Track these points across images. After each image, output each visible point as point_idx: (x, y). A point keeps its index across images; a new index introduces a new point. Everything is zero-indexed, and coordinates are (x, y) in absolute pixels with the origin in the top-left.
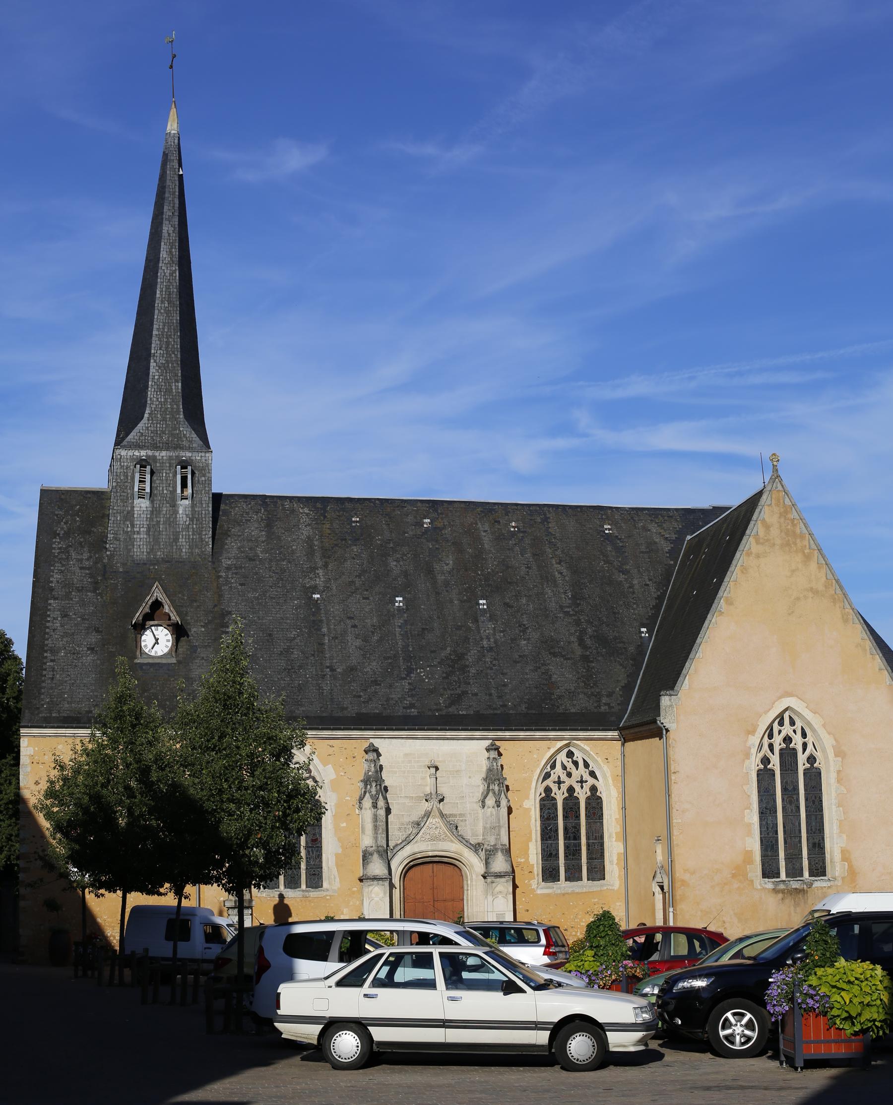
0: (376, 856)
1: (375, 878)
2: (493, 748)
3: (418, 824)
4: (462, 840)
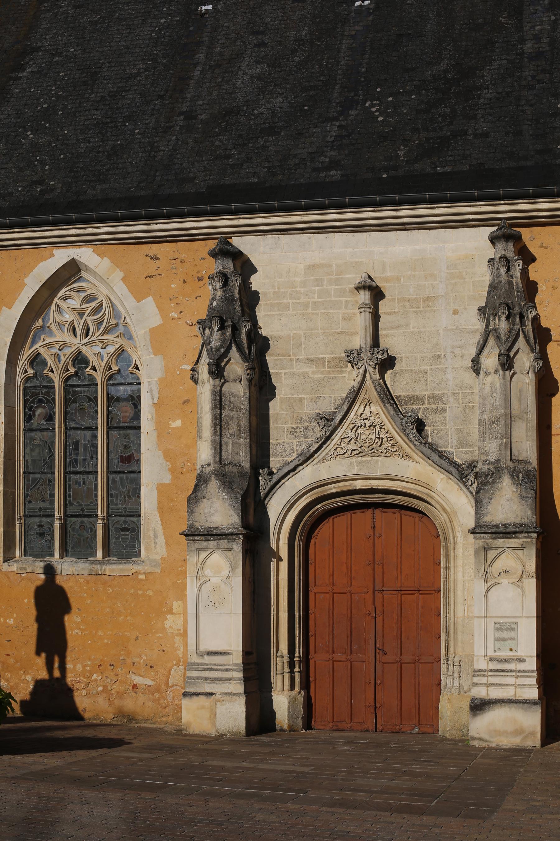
0: (214, 485)
1: (212, 534)
2: (507, 234)
3: (329, 423)
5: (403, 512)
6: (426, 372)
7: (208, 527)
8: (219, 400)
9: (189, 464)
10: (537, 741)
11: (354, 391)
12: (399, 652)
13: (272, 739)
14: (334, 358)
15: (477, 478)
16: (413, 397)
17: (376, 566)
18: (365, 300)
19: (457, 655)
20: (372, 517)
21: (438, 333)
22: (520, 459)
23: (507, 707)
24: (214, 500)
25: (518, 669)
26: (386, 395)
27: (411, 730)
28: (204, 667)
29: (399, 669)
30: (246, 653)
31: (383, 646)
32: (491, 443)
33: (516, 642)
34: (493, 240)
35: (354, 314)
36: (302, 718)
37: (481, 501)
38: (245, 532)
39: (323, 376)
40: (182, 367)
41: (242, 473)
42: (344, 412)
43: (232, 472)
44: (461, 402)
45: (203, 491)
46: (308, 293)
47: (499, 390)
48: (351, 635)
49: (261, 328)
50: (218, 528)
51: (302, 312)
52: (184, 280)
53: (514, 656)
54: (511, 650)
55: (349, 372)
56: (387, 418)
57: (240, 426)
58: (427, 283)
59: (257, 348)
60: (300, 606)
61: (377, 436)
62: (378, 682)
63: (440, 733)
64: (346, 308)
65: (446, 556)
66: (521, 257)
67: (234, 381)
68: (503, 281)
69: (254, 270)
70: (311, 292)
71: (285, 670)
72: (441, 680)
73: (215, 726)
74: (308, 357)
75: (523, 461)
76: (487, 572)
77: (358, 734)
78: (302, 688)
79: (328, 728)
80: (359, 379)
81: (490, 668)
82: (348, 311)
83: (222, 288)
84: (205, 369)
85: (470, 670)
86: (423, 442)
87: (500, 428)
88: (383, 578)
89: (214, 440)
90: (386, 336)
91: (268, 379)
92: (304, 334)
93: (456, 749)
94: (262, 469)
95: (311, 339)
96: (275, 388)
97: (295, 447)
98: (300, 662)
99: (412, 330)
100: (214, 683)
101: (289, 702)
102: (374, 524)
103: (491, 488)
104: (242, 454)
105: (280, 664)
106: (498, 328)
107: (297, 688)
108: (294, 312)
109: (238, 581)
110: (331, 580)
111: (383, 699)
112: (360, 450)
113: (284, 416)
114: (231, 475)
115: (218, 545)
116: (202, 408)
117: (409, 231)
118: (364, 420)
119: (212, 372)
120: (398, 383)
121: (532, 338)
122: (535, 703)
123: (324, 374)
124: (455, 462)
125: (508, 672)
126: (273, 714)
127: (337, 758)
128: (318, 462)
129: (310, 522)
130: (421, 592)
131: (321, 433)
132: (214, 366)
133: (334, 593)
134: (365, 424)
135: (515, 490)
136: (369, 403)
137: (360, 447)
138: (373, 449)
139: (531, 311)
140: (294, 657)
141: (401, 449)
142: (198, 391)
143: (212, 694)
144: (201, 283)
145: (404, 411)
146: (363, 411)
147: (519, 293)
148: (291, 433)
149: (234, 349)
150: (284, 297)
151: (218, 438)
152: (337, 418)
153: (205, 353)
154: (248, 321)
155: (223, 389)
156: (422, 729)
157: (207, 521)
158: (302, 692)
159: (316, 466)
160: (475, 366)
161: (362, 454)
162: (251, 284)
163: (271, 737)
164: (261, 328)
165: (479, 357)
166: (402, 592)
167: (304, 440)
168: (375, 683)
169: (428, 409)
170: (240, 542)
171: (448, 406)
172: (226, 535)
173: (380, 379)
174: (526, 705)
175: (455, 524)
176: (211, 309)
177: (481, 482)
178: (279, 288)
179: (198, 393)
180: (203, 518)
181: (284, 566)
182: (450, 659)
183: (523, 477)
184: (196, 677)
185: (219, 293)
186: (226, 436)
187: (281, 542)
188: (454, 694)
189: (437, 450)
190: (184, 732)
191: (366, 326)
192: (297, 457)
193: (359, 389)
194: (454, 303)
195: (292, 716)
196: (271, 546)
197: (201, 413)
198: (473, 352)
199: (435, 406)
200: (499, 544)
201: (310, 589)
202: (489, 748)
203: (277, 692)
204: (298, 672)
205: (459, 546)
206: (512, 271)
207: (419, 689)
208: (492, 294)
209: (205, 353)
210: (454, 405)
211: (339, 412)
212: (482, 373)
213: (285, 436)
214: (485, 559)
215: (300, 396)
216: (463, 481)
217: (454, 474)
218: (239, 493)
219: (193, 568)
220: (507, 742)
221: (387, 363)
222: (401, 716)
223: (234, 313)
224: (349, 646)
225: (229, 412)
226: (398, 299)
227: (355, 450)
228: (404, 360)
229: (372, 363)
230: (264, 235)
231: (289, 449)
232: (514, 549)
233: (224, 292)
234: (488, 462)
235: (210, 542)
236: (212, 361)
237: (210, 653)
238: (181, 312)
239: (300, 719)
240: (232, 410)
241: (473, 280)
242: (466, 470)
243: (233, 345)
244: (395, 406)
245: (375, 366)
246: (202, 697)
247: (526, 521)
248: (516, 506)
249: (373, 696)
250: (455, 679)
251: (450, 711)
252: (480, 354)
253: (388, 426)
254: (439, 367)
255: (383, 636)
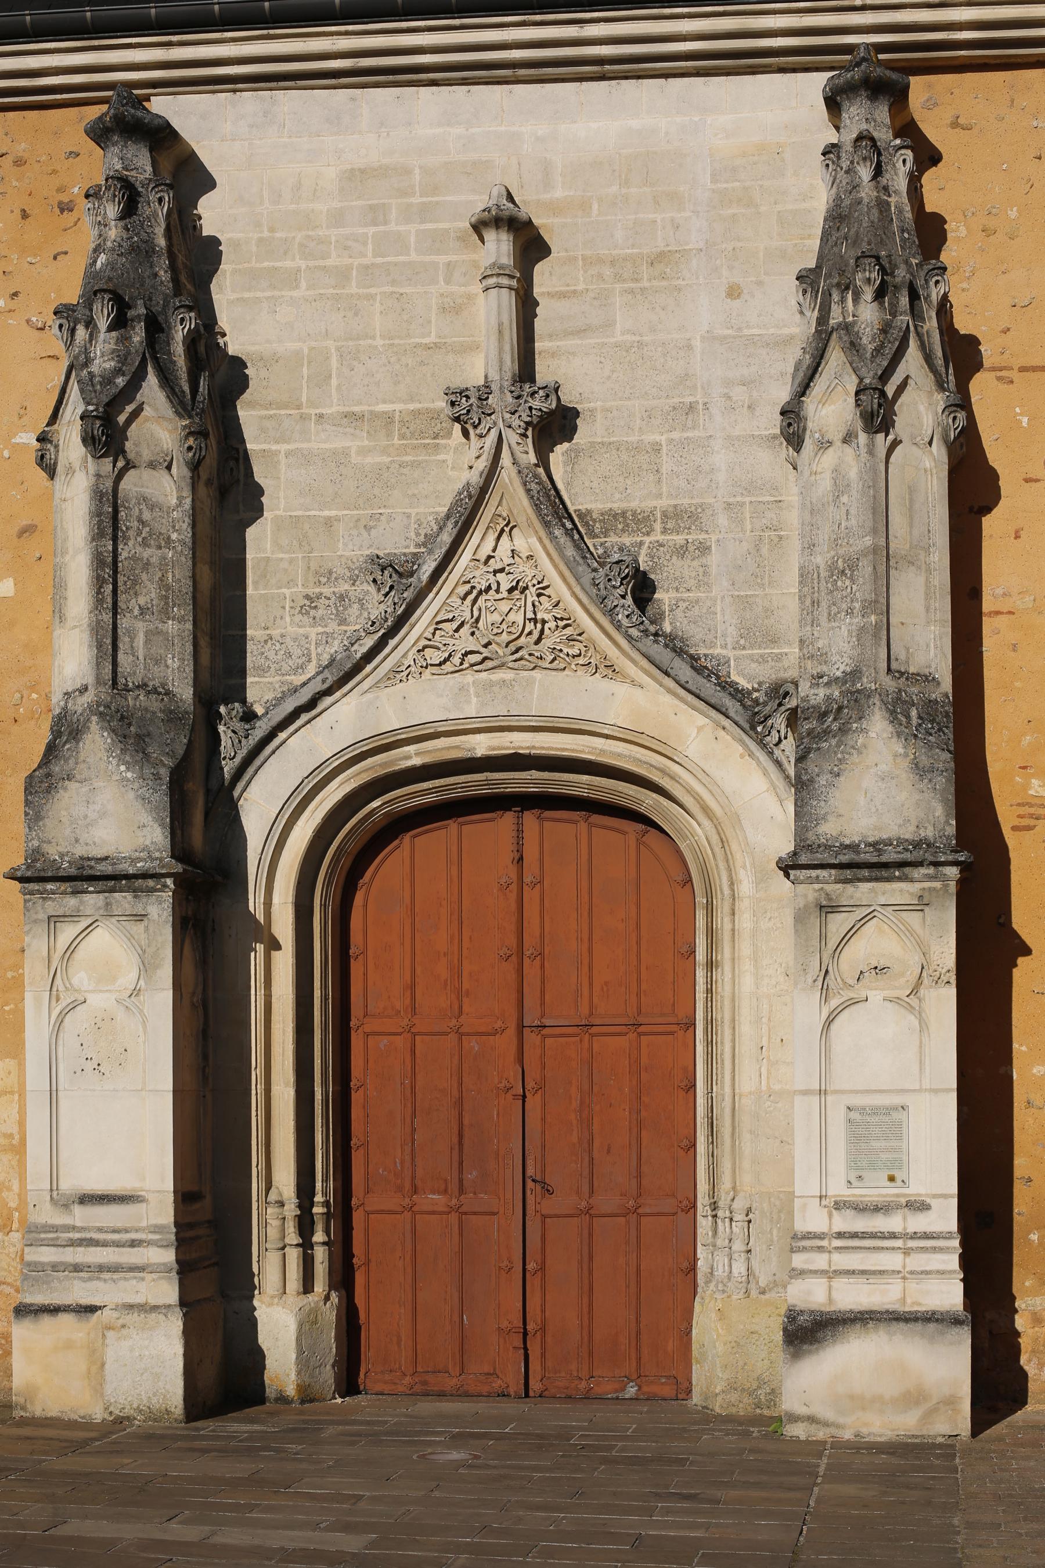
0: (96, 744)
3: (405, 584)
4: (703, 680)
5: (596, 818)
6: (656, 448)
7: (82, 858)
8: (110, 517)
9: (34, 696)
10: (963, 1424)
11: (470, 497)
12: (586, 1188)
13: (256, 1427)
14: (416, 413)
15: (794, 724)
16: (624, 513)
17: (527, 962)
18: (498, 257)
19: (741, 1195)
20: (515, 834)
21: (690, 347)
22: (912, 670)
23: (881, 1333)
24: (98, 784)
25: (911, 1230)
26: (552, 507)
27: (616, 1391)
28: (71, 1235)
29: (586, 1232)
30: (185, 1197)
31: (543, 1172)
32: (833, 628)
33: (905, 1158)
34: (833, 103)
35: (470, 297)
36: (333, 1366)
37: (812, 781)
38: (179, 868)
39: (386, 459)
40: (17, 440)
41: (171, 712)
42: (444, 550)
43: (146, 709)
44: (748, 527)
45: (66, 760)
46: (349, 243)
47: (856, 486)
48: (460, 1143)
49: (224, 335)
50: (106, 858)
51: (331, 291)
52: (24, 211)
53: (898, 1195)
54: (892, 1179)
55: (456, 449)
56: (556, 566)
57: (168, 587)
58: (658, 217)
59: (214, 386)
60: (327, 1068)
61: (530, 615)
62: (531, 1266)
63: (696, 1399)
64: (448, 282)
65: (711, 932)
66: (908, 142)
67: (152, 465)
68: (866, 200)
69: (208, 183)
70: (357, 241)
71: (287, 1241)
72: (695, 1260)
73: (102, 1395)
74: (347, 409)
75: (918, 675)
76: (827, 972)
77: (481, 1407)
78: (332, 1286)
79: (401, 1389)
80: (482, 464)
81: (836, 1229)
82: (454, 288)
83: (121, 219)
84: (74, 434)
85: (775, 1232)
86: (652, 629)
87: (862, 587)
88: (543, 993)
89: (98, 622)
90: (553, 355)
91: (242, 467)
92: (338, 349)
93: (752, 1451)
94: (226, 705)
95: (355, 363)
96: (260, 491)
97: (313, 647)
98: (328, 1216)
99: (620, 338)
100: (98, 1279)
101: (300, 1326)
102: (520, 850)
103: (838, 746)
104: (173, 663)
105: (274, 1223)
106: (854, 323)
107: (320, 1285)
108: (311, 292)
109: (161, 1001)
110: (408, 1001)
111: (543, 1311)
112: (486, 653)
113: (284, 565)
114: (142, 718)
115: (107, 904)
116: (65, 540)
117: (614, 82)
118: (495, 572)
119: (93, 437)
120: (583, 476)
121: (939, 353)
122: (957, 1322)
123: (389, 455)
124: (733, 684)
125: (885, 1238)
126: (257, 1357)
127: (437, 1494)
128: (376, 685)
129: (353, 847)
130: (642, 1029)
131: (383, 607)
132: (98, 423)
133: (415, 1035)
134: (498, 584)
135: (901, 751)
136: (508, 528)
137: (486, 646)
138: (523, 650)
139: (937, 282)
140: (312, 1204)
141: (592, 650)
142: (57, 495)
143: (92, 1309)
144: (69, 218)
145: (601, 551)
146: (494, 551)
147: (906, 235)
148: (303, 611)
149: (152, 379)
150: (285, 253)
151: (107, 617)
152: (425, 568)
153: (74, 391)
154: (190, 309)
155: (123, 485)
156: (645, 1389)
157: (77, 841)
158: (334, 1297)
159: (369, 696)
160: (790, 425)
161: (489, 664)
162: (200, 218)
163: (252, 1421)
164: (224, 335)
165: (800, 402)
166: (594, 1030)
167: (337, 628)
168: (524, 1270)
169: (662, 545)
170: (167, 896)
171: (714, 538)
172: (127, 877)
173: (537, 465)
174: (932, 1326)
175: (734, 847)
176: (91, 275)
177: (810, 732)
178: (272, 230)
179: (57, 501)
180: (68, 831)
181: (284, 963)
182: (721, 1204)
183: (920, 717)
184: (48, 1264)
185: (113, 233)
186: (131, 611)
187: (276, 900)
188: (734, 1297)
189: (686, 653)
190: (17, 1413)
191: (500, 325)
192: (318, 674)
193: (484, 490)
194: (731, 268)
195: (308, 1361)
196: (251, 909)
197: (64, 553)
198: (783, 394)
199: (679, 539)
200: (858, 895)
201: (352, 1024)
202: (838, 1445)
203: (267, 1299)
204: (324, 1243)
205: (744, 906)
206: (887, 176)
207: (638, 1283)
208: (835, 235)
209: (74, 391)
210: (730, 535)
211: (431, 552)
212: (808, 442)
213: (288, 619)
214: (823, 937)
215: (327, 513)
216: (757, 733)
217: (732, 714)
218: (164, 765)
219: (41, 968)
220: (883, 1425)
221: (555, 425)
222: (591, 1354)
223: (153, 287)
224: (455, 1174)
225: (139, 549)
226: (584, 259)
227: (472, 652)
228: (599, 416)
229: (516, 423)
230: (235, 91)
231: (297, 652)
232: (900, 908)
233: (128, 230)
234: (825, 679)
235: (87, 897)
236: (91, 408)
237: (87, 1199)
238: (15, 294)
239: (329, 1367)
240: (145, 544)
241: (779, 207)
242: (765, 704)
243: (150, 369)
244: (577, 536)
245: (526, 429)
246: (66, 1320)
247: (929, 833)
248: (904, 795)
249: (519, 1305)
250: (735, 1256)
251: (726, 1345)
252: (803, 394)
253: (559, 588)
254: (690, 434)
255: (543, 1147)
